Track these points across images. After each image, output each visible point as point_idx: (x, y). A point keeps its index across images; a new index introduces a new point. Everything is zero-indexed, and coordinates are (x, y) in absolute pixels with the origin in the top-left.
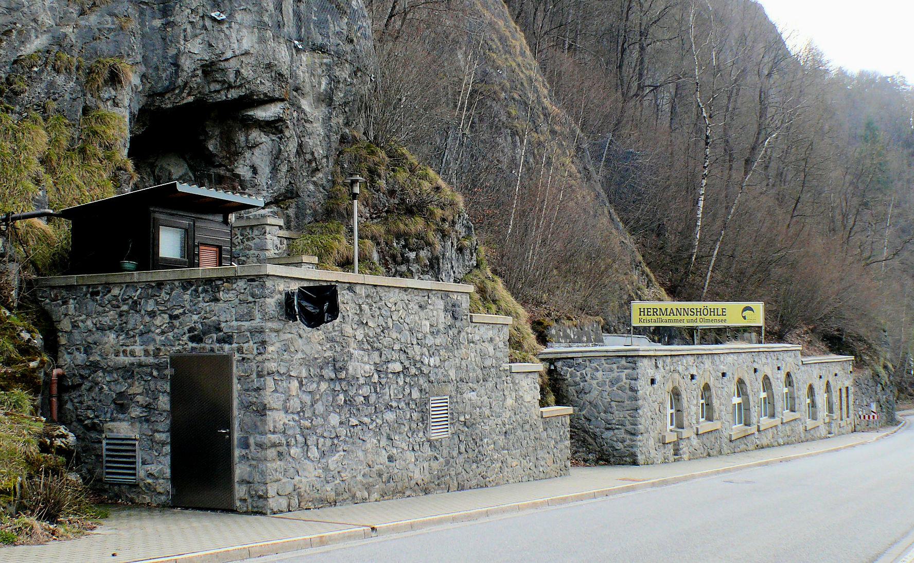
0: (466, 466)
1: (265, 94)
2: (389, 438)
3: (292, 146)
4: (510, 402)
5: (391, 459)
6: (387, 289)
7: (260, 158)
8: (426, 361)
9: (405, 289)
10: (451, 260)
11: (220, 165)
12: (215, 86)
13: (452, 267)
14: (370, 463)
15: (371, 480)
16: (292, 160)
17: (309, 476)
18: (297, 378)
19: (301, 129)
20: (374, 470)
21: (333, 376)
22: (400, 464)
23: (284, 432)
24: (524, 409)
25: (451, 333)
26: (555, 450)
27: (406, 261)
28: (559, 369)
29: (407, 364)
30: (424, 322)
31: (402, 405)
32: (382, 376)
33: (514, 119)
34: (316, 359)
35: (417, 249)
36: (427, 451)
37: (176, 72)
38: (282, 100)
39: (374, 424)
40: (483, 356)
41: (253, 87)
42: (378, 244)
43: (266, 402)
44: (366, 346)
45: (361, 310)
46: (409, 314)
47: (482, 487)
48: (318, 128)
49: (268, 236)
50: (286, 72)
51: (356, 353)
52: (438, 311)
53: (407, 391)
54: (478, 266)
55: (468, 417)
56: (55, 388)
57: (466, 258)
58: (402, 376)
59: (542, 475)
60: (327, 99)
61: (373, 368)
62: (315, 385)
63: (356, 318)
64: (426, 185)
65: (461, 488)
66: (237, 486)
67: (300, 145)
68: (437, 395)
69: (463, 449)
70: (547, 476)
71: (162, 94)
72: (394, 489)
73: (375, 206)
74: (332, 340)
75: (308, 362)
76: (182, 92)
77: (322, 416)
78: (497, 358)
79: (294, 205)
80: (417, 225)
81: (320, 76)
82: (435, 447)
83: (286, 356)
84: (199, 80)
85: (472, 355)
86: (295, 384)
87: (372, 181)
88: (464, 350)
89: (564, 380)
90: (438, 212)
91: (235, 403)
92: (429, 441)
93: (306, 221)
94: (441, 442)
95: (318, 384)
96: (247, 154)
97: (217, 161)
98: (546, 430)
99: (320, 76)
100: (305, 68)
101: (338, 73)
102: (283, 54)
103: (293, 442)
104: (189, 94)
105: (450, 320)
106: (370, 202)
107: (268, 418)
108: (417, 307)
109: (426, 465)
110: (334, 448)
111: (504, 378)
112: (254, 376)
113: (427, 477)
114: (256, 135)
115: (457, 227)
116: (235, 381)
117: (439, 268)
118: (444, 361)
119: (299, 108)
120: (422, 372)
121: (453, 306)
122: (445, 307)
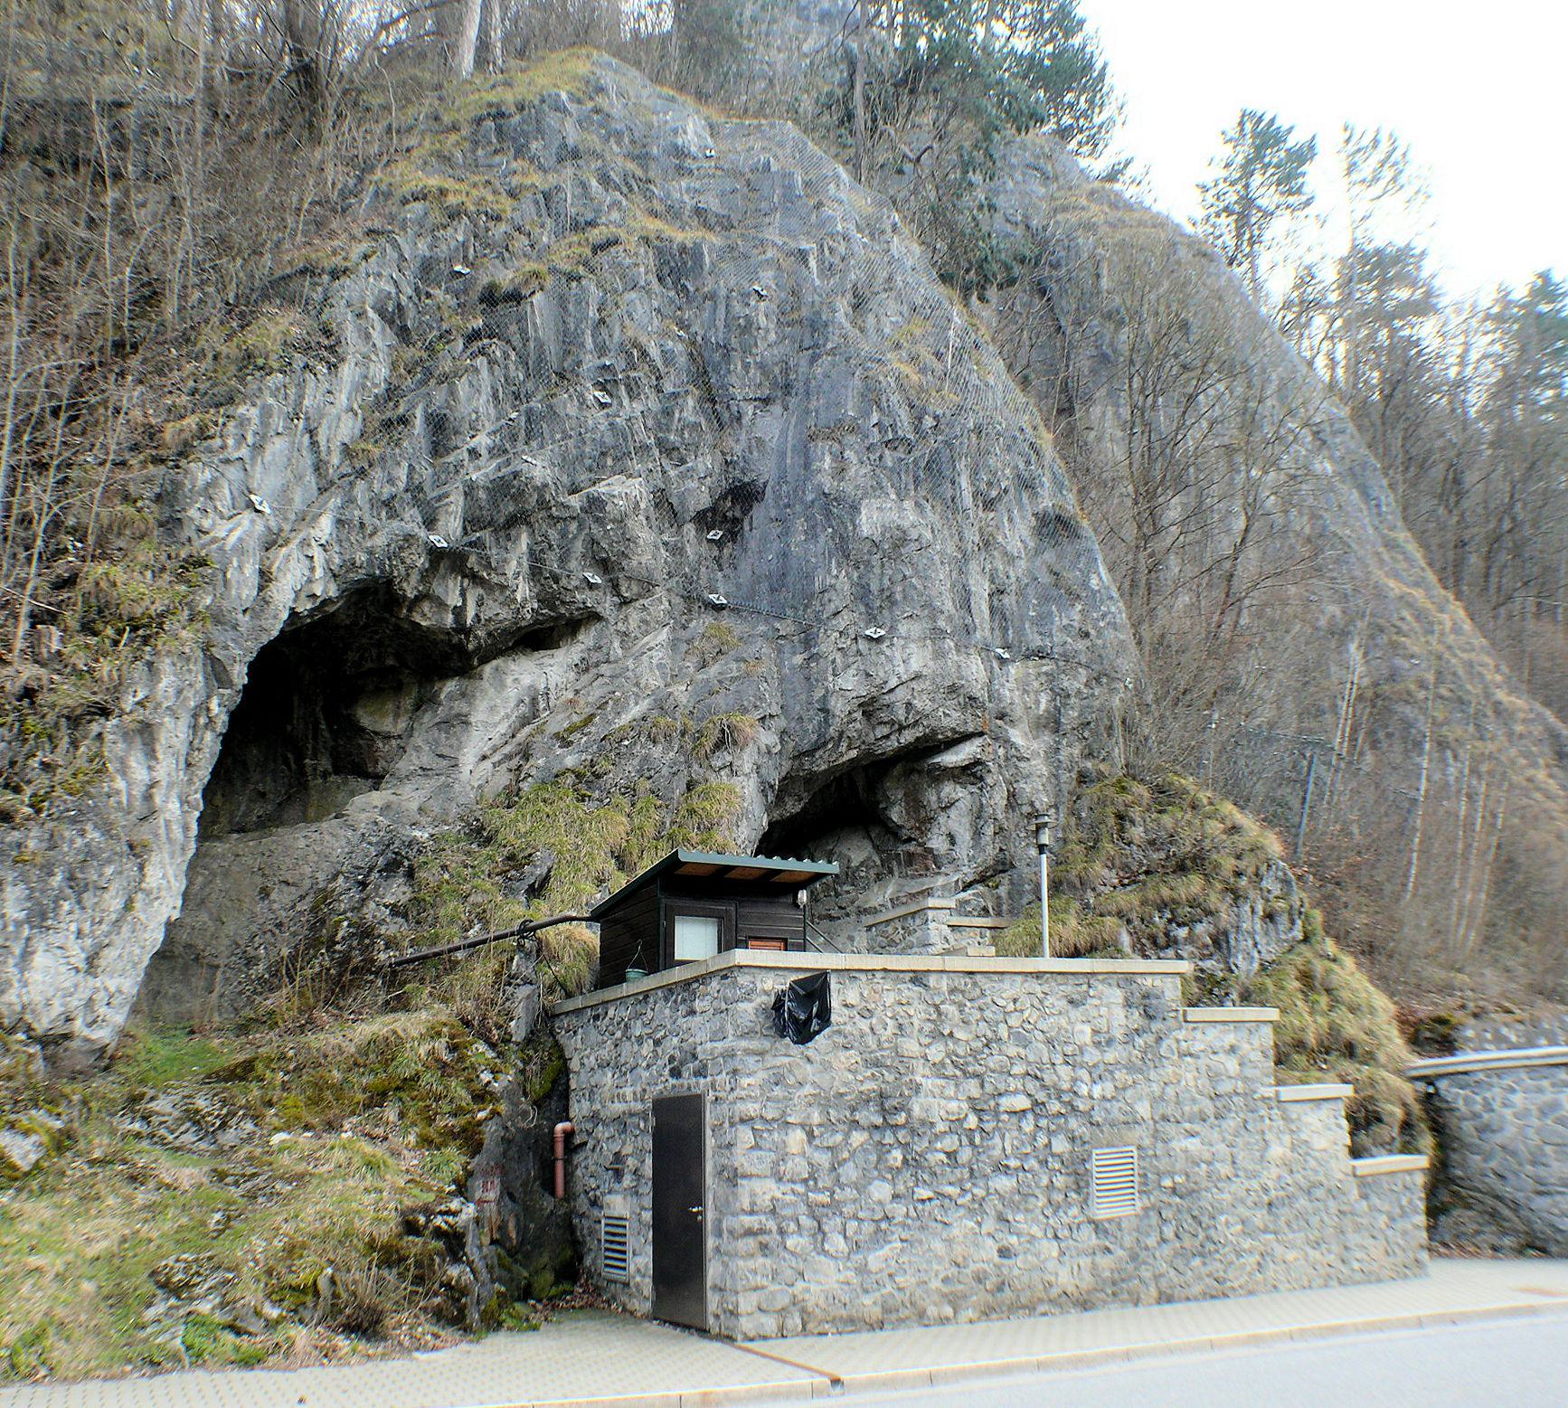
0: (1179, 1263)
1: (953, 730)
2: (1002, 1219)
3: (999, 798)
4: (1277, 1151)
5: (1004, 1252)
6: (995, 977)
7: (957, 821)
8: (1084, 1090)
9: (1038, 975)
10: (1252, 934)
11: (910, 840)
12: (882, 731)
13: (1256, 945)
14: (960, 1260)
15: (961, 1287)
16: (1000, 817)
17: (826, 1280)
18: (802, 1126)
19: (1013, 771)
20: (968, 1271)
21: (879, 1121)
22: (1025, 1261)
23: (773, 1211)
24: (1313, 1163)
25: (1139, 1041)
26: (1390, 1233)
27: (1171, 942)
28: (1442, 1093)
29: (1041, 1096)
30: (1079, 1026)
31: (1032, 1163)
32: (986, 1118)
33: (1442, 725)
34: (842, 1095)
35: (1189, 923)
36: (1087, 1237)
37: (826, 720)
38: (981, 734)
39: (969, 1197)
40: (1214, 1077)
41: (934, 723)
42: (1129, 922)
43: (736, 1164)
44: (950, 1070)
45: (940, 1014)
46: (1045, 1016)
47: (1213, 1297)
48: (1039, 766)
49: (932, 925)
50: (982, 694)
51: (928, 1084)
52: (1111, 1009)
53: (1042, 1140)
54: (1306, 940)
55: (1178, 1179)
56: (560, 1148)
57: (1281, 928)
58: (1030, 1116)
59: (1358, 1276)
60: (1052, 723)
61: (965, 1106)
62: (839, 1137)
63: (928, 1027)
64: (1214, 827)
65: (1165, 1298)
66: (709, 1293)
67: (1012, 795)
68: (1108, 1146)
69: (1169, 1232)
70: (1371, 1278)
71: (810, 753)
72: (1004, 1301)
73: (1125, 867)
74: (877, 1064)
75: (823, 1101)
76: (837, 745)
77: (856, 1186)
78: (1246, 1080)
79: (1006, 881)
80: (1193, 884)
81: (1037, 692)
82: (1106, 1231)
83: (778, 1092)
84: (858, 726)
85: (1189, 1076)
86: (799, 1135)
87: (1122, 830)
88: (1170, 1070)
89: (1452, 1110)
90: (1229, 864)
91: (709, 1167)
92: (1091, 1221)
93: (1025, 901)
94: (1119, 1224)
95: (847, 1135)
96: (942, 819)
97: (905, 833)
98: (1365, 1197)
99: (1037, 692)
100: (1019, 687)
101: (1066, 684)
102: (975, 671)
103: (793, 1226)
104: (849, 748)
105: (1136, 1018)
106: (1117, 862)
107: (740, 1190)
108: (1064, 1002)
109: (1085, 1262)
110: (879, 1237)
111: (1263, 1112)
112: (727, 1125)
113: (1087, 1281)
114: (950, 790)
115: (1267, 883)
116: (709, 1132)
117: (1229, 948)
118: (1124, 1089)
119: (1007, 742)
120: (1074, 1109)
121: (1146, 996)
122: (1126, 999)
